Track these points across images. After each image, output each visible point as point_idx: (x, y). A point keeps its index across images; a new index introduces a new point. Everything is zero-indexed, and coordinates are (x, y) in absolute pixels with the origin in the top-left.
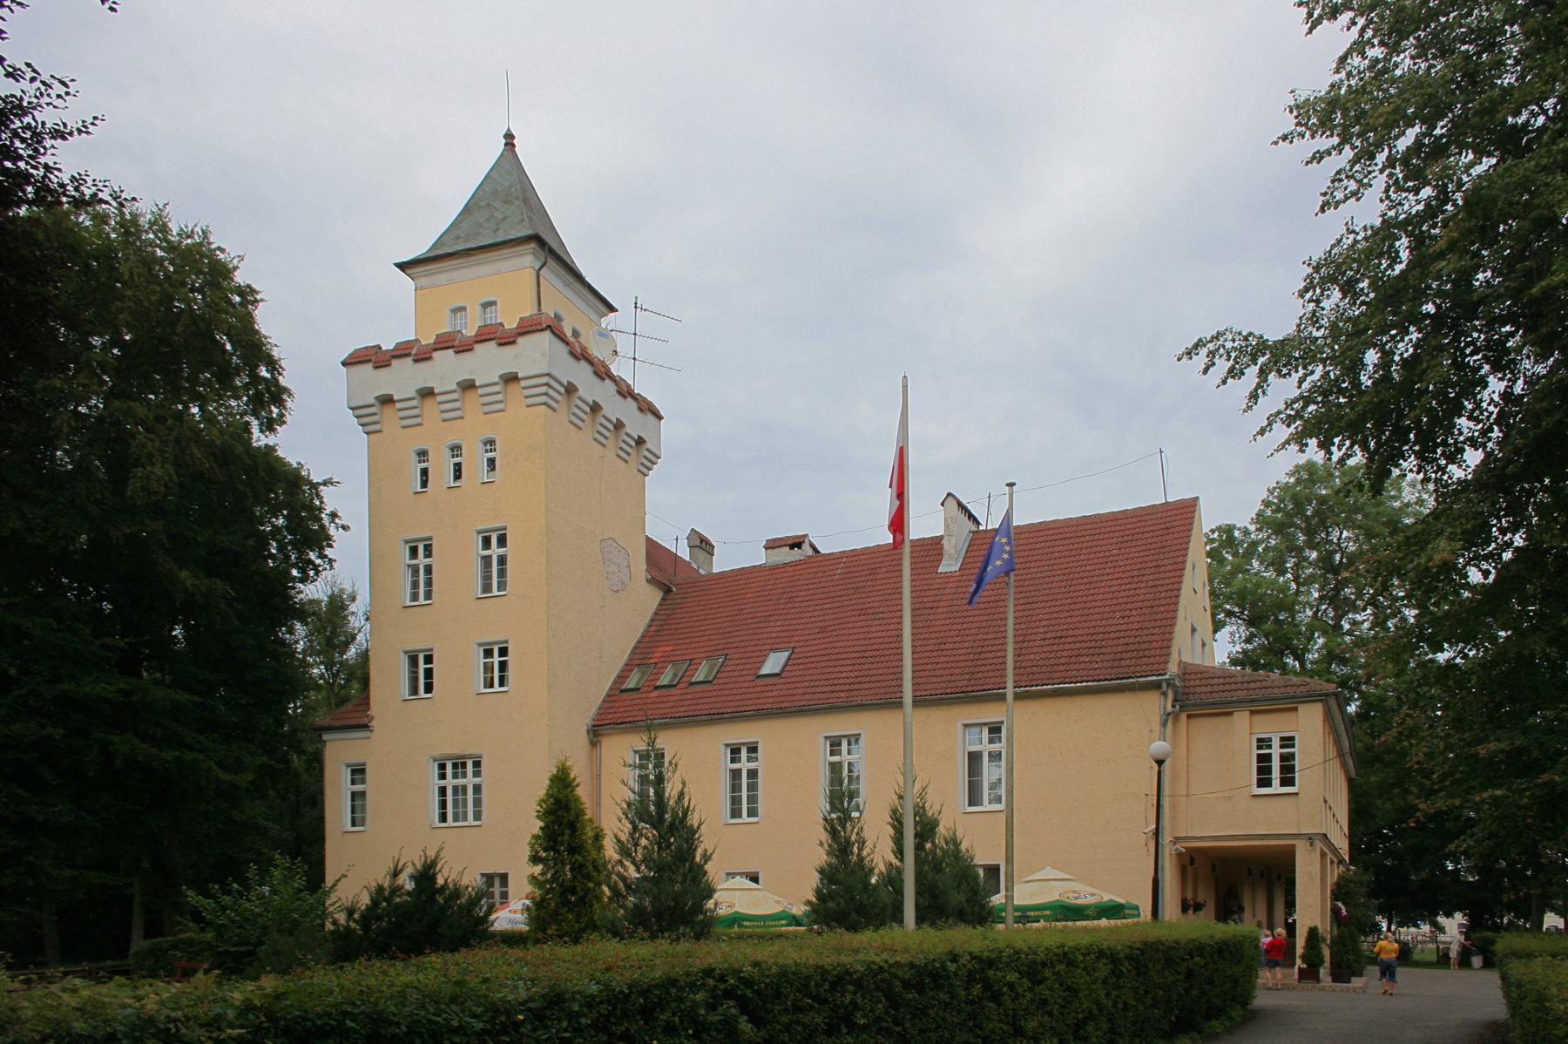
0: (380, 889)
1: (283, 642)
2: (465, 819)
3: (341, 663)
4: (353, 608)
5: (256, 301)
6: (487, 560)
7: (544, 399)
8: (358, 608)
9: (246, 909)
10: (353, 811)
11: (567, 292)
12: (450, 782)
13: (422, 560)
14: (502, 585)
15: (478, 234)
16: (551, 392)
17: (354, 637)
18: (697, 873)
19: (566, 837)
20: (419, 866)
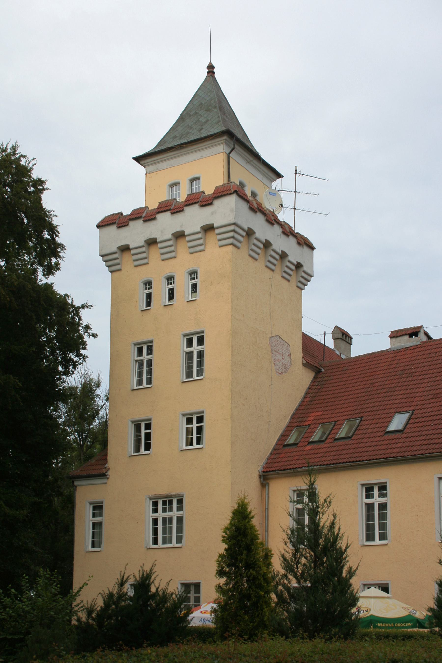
0: (111, 595)
1: (50, 417)
2: (171, 542)
3: (89, 430)
4: (98, 392)
5: (44, 189)
6: (190, 355)
7: (231, 241)
8: (102, 391)
9: (19, 608)
10: (93, 537)
11: (248, 167)
12: (160, 515)
13: (145, 357)
14: (200, 372)
15: (188, 133)
16: (237, 236)
17: (98, 412)
18: (344, 586)
19: (244, 557)
20: (138, 579)
